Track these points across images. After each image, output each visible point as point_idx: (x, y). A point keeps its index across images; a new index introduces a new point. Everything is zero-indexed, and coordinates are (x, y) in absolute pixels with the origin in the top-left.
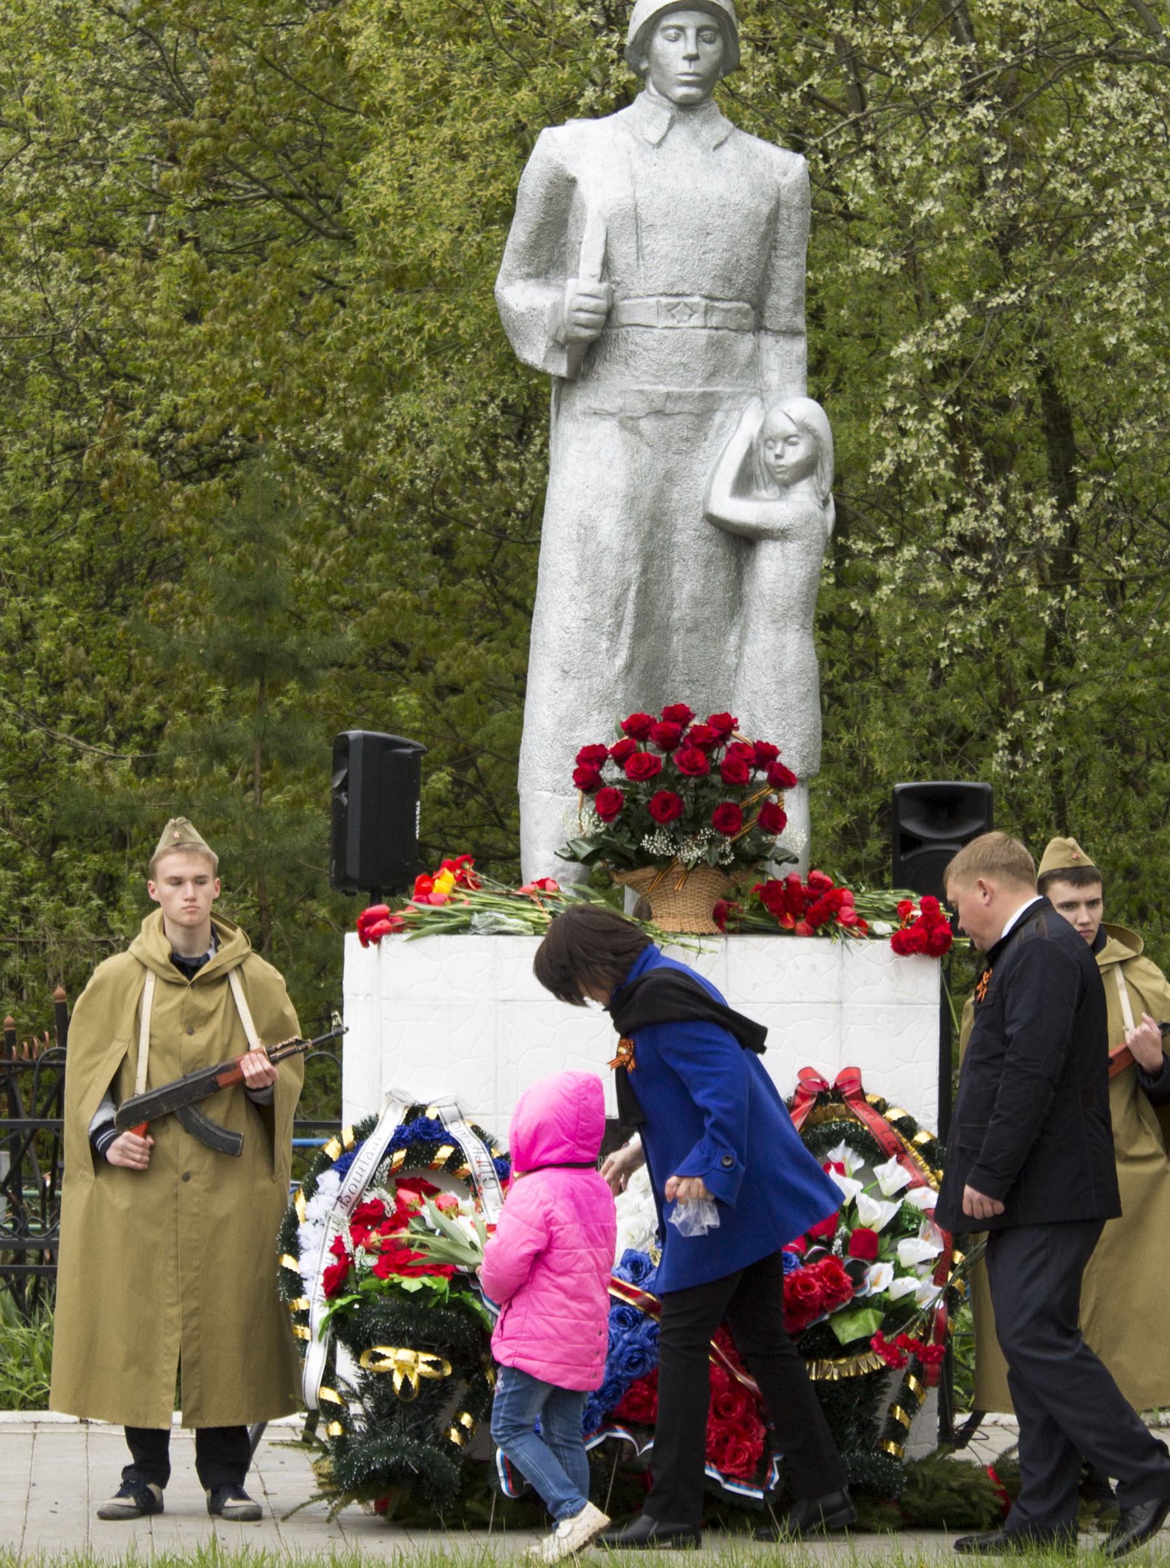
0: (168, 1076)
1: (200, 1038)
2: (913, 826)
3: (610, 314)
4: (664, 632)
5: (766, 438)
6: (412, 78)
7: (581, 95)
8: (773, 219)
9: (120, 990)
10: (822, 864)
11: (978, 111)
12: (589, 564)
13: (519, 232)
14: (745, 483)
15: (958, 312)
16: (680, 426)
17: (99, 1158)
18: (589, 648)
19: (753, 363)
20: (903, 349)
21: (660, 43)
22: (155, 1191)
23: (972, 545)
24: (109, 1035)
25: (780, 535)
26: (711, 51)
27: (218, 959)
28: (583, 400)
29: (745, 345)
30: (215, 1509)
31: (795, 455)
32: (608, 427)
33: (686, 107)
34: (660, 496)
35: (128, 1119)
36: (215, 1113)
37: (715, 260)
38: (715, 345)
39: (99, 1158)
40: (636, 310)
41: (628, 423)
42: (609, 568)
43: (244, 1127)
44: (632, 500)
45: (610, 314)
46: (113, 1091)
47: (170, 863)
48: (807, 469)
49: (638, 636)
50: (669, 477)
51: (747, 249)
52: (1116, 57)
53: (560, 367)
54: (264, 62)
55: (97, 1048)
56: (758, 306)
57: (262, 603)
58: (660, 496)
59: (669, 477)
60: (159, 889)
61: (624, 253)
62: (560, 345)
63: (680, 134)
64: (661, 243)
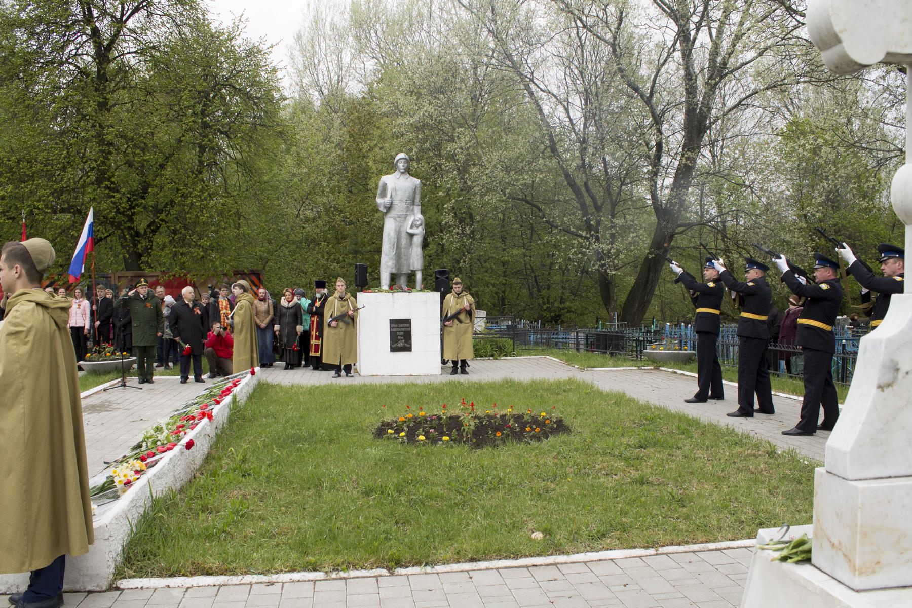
0: (339, 314)
1: (344, 309)
2: (438, 276)
3: (392, 203)
4: (401, 249)
5: (415, 220)
6: (377, 169)
7: (854, 188)
8: (415, 189)
9: (332, 302)
10: (401, 288)
11: (455, 172)
12: (389, 239)
13: (379, 192)
14: (412, 227)
15: (454, 201)
16: (403, 219)
17: (329, 325)
18: (389, 251)
19: (413, 210)
20: (445, 206)
21: (399, 164)
22: (337, 331)
23: (458, 233)
24: (331, 308)
25: (417, 234)
26: (406, 165)
27: (346, 297)
28: (389, 215)
29: (412, 207)
30: (347, 376)
31: (419, 223)
32: (392, 219)
33: (402, 173)
34: (400, 229)
35: (334, 320)
36: (346, 319)
37: (407, 195)
38: (407, 207)
39: (329, 325)
40: (395, 202)
41: (395, 219)
42: (392, 240)
43: (350, 321)
44: (395, 230)
45: (392, 203)
46: (331, 316)
47: (338, 283)
48: (421, 225)
49: (397, 249)
50: (401, 226)
51: (411, 194)
52: (475, 165)
53: (385, 211)
54: (358, 166)
55: (329, 310)
56: (413, 201)
57: (356, 244)
58: (400, 229)
59: (401, 226)
60: (337, 287)
61: (394, 194)
62: (385, 207)
63: (402, 177)
64: (399, 193)
